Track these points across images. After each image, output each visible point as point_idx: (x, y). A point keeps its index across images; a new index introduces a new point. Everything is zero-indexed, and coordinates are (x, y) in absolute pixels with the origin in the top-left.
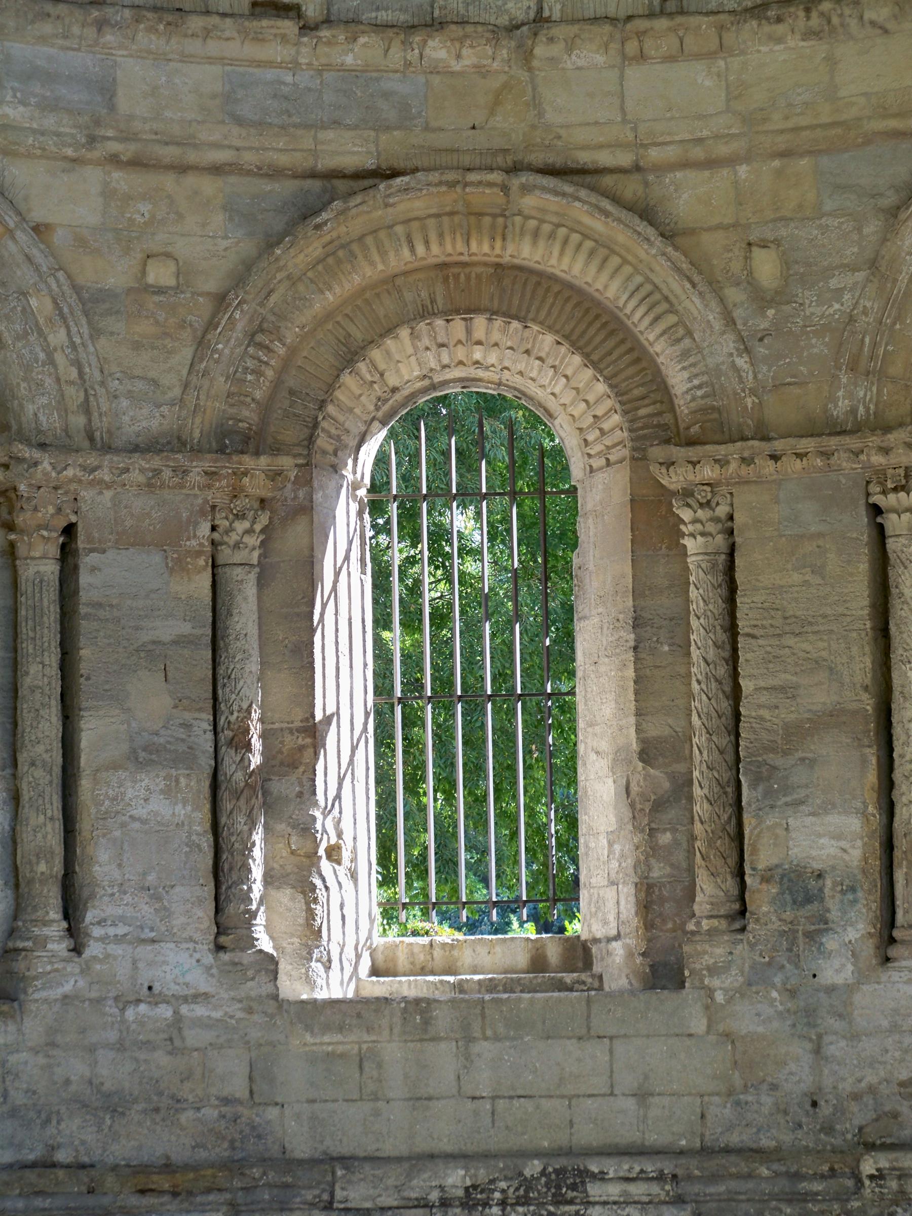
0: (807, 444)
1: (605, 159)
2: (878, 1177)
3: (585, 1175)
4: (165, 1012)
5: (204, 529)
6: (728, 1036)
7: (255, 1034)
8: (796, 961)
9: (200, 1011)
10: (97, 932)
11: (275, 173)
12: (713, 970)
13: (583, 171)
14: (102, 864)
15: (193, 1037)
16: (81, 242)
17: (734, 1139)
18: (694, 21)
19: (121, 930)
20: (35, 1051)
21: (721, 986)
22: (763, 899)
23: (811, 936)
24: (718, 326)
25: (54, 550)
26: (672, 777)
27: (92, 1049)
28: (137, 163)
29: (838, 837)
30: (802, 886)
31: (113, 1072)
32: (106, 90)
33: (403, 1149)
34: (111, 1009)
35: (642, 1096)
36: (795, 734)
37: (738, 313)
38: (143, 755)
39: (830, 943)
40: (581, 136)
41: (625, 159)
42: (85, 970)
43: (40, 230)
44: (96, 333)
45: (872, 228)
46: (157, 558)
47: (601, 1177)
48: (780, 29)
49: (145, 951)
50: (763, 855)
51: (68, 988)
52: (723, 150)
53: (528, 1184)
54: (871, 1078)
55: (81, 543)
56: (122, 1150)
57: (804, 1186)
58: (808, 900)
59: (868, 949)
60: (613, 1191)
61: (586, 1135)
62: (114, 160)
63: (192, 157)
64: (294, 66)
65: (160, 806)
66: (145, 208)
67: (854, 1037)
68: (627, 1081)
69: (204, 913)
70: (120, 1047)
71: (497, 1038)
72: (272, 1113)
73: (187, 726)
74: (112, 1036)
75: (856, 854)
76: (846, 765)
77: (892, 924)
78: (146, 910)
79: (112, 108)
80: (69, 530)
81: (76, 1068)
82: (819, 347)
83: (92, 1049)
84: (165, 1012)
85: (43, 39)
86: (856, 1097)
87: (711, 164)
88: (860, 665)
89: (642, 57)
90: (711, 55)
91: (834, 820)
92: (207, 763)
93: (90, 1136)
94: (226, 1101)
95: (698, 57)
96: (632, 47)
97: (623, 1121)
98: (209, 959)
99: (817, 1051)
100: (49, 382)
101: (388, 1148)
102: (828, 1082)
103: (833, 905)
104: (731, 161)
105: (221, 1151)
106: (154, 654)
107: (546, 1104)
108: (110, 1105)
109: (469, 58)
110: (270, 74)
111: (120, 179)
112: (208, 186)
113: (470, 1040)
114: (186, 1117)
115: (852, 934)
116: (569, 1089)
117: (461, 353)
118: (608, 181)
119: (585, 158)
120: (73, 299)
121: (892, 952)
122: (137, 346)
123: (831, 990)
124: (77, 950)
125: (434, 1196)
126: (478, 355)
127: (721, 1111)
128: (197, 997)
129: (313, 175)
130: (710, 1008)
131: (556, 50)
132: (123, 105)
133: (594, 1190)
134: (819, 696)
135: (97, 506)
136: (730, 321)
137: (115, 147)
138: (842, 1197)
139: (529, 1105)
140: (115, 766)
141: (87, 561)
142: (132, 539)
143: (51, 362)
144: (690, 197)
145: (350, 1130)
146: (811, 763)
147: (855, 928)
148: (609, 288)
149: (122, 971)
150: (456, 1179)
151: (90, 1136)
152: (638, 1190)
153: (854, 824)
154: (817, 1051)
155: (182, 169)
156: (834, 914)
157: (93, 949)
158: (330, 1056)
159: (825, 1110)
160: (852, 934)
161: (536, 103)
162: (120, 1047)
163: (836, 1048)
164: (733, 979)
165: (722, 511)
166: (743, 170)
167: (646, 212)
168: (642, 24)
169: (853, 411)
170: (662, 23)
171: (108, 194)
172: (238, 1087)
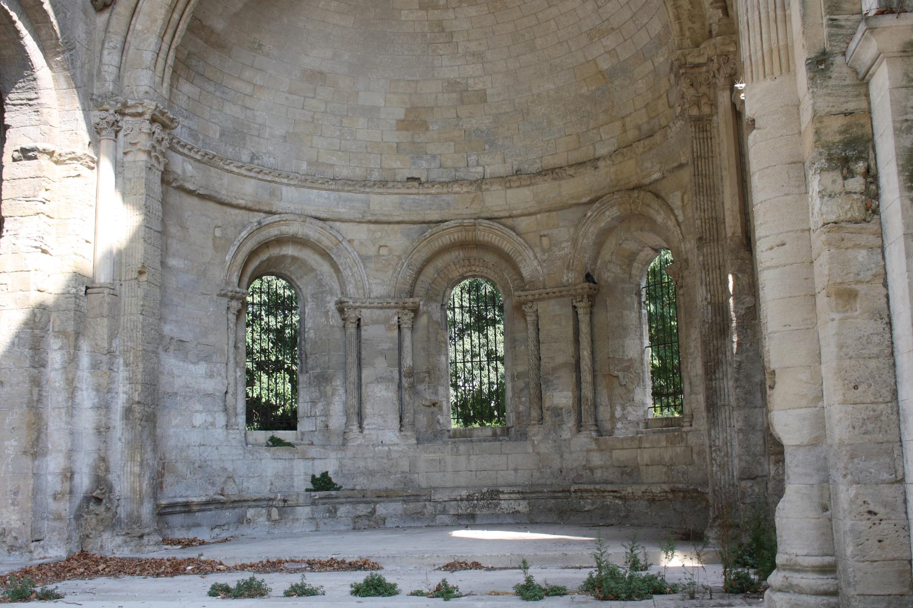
0: (555, 290)
1: (502, 214)
2: (575, 492)
3: (499, 492)
4: (386, 448)
5: (396, 318)
6: (538, 453)
7: (411, 454)
8: (556, 432)
9: (396, 448)
10: (366, 427)
11: (414, 223)
12: (534, 435)
13: (496, 218)
14: (368, 410)
15: (394, 455)
16: (362, 244)
17: (540, 481)
18: (523, 176)
19: (374, 426)
20: (350, 459)
21: (536, 439)
22: (547, 416)
23: (559, 425)
24: (532, 258)
25: (355, 325)
26: (525, 382)
27: (366, 459)
28: (376, 222)
29: (566, 398)
30: (557, 412)
31: (372, 465)
32: (367, 203)
33: (452, 485)
34: (371, 447)
35: (516, 470)
36: (555, 369)
37: (538, 255)
38: (380, 380)
39: (564, 427)
40: (495, 209)
41: (507, 214)
42: (364, 437)
43: (350, 241)
44: (365, 267)
45: (572, 230)
46: (383, 326)
47: (503, 493)
48: (546, 177)
49: (380, 432)
50: (547, 403)
51: (359, 442)
52: (532, 210)
53: (483, 494)
54: (575, 464)
55: (362, 323)
56: (374, 486)
57: (557, 495)
58: (559, 415)
59: (574, 429)
60: (506, 496)
61: (501, 481)
62: (370, 222)
63: (391, 219)
64: (418, 194)
65: (384, 393)
66: (379, 234)
67: (571, 453)
68: (512, 466)
69: (397, 422)
70: (373, 458)
71: (476, 454)
72: (416, 476)
73: (391, 372)
74: (371, 455)
75: (571, 402)
76: (566, 378)
77: (581, 421)
78: (380, 421)
79: (369, 207)
80: (359, 320)
81: (362, 464)
82: (559, 263)
83: (366, 459)
84: (386, 448)
85: (349, 191)
86: (572, 470)
87: (530, 214)
88: (571, 349)
89: (510, 187)
90: (529, 185)
91: (565, 393)
92: (397, 381)
93: (365, 482)
94: (403, 472)
95: (526, 186)
96: (508, 185)
97: (510, 477)
98: (398, 434)
99: (562, 457)
100: (353, 281)
101: (448, 485)
102: (564, 465)
103: (565, 416)
104: (535, 214)
105: (402, 486)
106: (383, 353)
107: (490, 473)
108: (372, 473)
109: (465, 189)
110: (412, 197)
111: (372, 226)
112: (396, 227)
113: (469, 455)
114: (392, 477)
115: (570, 425)
116: (496, 468)
117: (469, 268)
118: (503, 220)
119: (496, 215)
120: (359, 259)
121: (582, 429)
122: (377, 270)
123: (565, 440)
124: (362, 432)
125: (459, 498)
126: (474, 268)
127: (537, 474)
128: (395, 445)
129: (424, 223)
130: (533, 445)
131: (488, 187)
132: (372, 207)
133: (501, 496)
134: (560, 359)
135: (366, 314)
136: (536, 257)
137: (370, 218)
138: (567, 498)
139: (485, 473)
140: (371, 383)
141: (363, 328)
142: (375, 322)
143: (353, 275)
144: (523, 224)
145: (437, 479)
146: (558, 378)
147: (570, 422)
148: (507, 247)
149: (374, 437)
150: (464, 493)
151: (365, 482)
152: (513, 496)
153: (570, 394)
154: (562, 457)
155: (389, 223)
156: (565, 419)
157: (366, 432)
158: (432, 460)
159: (564, 474)
160: (570, 425)
161: (483, 201)
162: (373, 458)
163: (566, 456)
164: (539, 437)
165: (535, 309)
166: (539, 216)
167: (512, 229)
168: (510, 178)
169: (568, 280)
170: (515, 178)
171: (369, 230)
172: (406, 469)
